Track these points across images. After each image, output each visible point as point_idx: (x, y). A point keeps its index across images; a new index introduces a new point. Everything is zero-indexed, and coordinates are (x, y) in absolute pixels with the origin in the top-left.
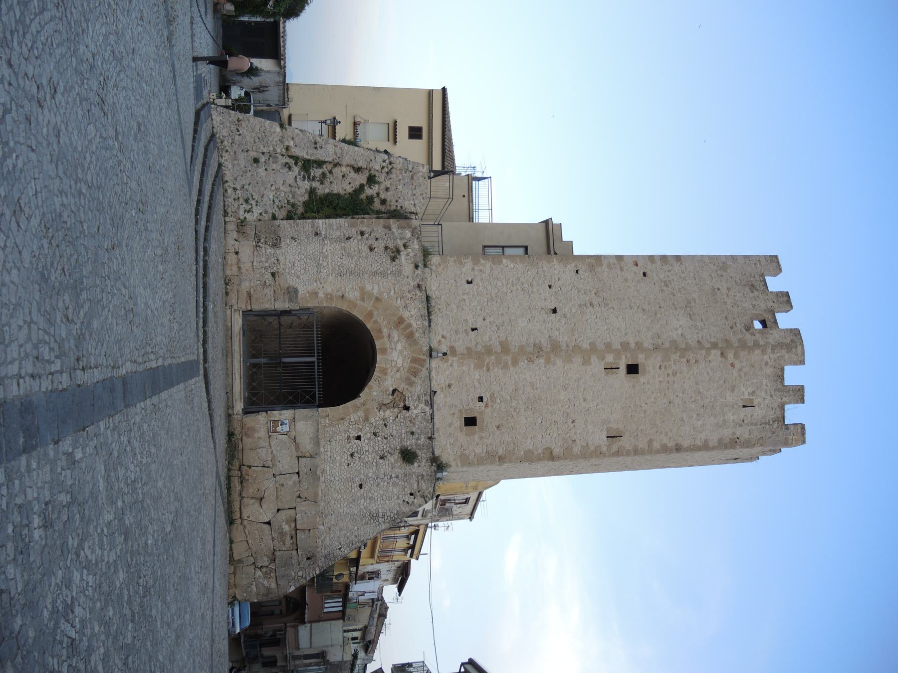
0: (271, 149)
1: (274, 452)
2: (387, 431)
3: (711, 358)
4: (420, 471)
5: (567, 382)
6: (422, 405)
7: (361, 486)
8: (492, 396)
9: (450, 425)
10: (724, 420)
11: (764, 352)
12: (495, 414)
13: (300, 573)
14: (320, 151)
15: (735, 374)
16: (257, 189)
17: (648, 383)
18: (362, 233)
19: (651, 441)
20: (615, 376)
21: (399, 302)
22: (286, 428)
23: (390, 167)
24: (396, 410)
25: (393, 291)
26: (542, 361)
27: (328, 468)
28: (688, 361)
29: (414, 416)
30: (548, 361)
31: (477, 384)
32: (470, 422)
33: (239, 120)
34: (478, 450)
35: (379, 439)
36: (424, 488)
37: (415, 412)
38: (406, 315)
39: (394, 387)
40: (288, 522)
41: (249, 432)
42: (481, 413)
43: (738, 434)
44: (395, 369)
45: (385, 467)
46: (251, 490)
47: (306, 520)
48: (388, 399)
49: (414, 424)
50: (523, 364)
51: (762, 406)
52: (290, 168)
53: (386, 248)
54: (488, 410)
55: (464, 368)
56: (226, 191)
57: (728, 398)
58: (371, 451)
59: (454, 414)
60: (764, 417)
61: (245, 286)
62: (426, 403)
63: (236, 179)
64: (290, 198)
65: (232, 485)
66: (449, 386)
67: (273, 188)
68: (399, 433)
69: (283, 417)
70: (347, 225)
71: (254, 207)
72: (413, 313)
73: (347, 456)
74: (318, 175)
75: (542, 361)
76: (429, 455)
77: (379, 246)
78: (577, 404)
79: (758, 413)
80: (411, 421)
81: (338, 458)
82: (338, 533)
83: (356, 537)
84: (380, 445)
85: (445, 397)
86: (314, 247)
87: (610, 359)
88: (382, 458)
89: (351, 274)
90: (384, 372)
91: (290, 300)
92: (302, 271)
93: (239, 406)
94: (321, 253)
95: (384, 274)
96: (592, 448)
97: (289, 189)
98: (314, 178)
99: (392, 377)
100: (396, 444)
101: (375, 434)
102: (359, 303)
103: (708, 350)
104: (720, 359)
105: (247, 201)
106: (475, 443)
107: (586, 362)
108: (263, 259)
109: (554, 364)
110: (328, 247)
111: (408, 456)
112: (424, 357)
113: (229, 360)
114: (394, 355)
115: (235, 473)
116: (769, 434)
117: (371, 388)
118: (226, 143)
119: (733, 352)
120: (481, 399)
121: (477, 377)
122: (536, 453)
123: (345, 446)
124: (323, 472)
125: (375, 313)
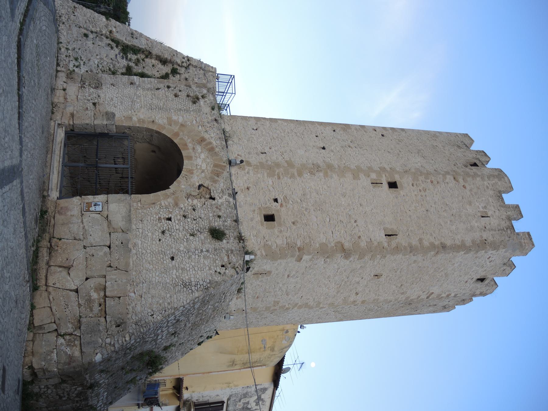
0: (98, 29)
1: (86, 227)
2: (196, 214)
3: (447, 181)
4: (229, 246)
5: (344, 191)
6: (226, 197)
7: (172, 258)
8: (285, 198)
9: (252, 220)
10: (471, 226)
11: (483, 179)
12: (290, 213)
13: (108, 340)
14: (135, 40)
15: (469, 193)
16: (85, 54)
17: (407, 195)
18: (168, 87)
19: (421, 240)
20: (380, 189)
21: (200, 128)
22: (99, 208)
23: (188, 63)
24: (203, 200)
25: (194, 122)
26: (321, 174)
27: (140, 242)
28: (432, 182)
29: (219, 204)
30: (326, 175)
31: (271, 189)
32: (269, 218)
33: (75, 7)
34: (279, 242)
35: (189, 220)
36: (235, 260)
37: (220, 201)
38: (206, 136)
39: (200, 183)
40: (97, 290)
41: (61, 211)
42: (278, 211)
43: (485, 237)
44: (200, 171)
45: (195, 243)
46: (59, 259)
47: (116, 287)
48: (196, 192)
49: (220, 210)
50: (307, 175)
51: (495, 217)
52: (112, 48)
53: (188, 96)
54: (283, 209)
55: (259, 175)
56: (60, 49)
57: (469, 210)
58: (181, 229)
59: (254, 211)
60: (499, 225)
61: (70, 109)
62: (229, 195)
63: (69, 43)
64: (111, 67)
65: (40, 254)
66: (248, 188)
67: (98, 57)
68: (206, 216)
69: (96, 200)
70: (156, 82)
71: (82, 65)
72: (212, 135)
73: (158, 234)
74: (133, 59)
75: (321, 174)
76: (236, 234)
77: (183, 95)
78: (356, 208)
79: (494, 222)
80: (217, 208)
81: (150, 234)
82: (150, 300)
83: (169, 304)
84: (190, 225)
85: (245, 196)
86: (130, 90)
87: (374, 176)
88: (192, 235)
89: (160, 109)
90: (191, 172)
91: (108, 119)
92: (119, 104)
93: (54, 194)
94: (135, 94)
95: (187, 111)
96: (376, 243)
97: (111, 61)
98: (130, 60)
99: (198, 176)
100: (205, 224)
101: (185, 216)
102: (167, 126)
103: (444, 176)
104: (454, 182)
105: (76, 59)
106: (275, 235)
107: (356, 177)
108: (87, 95)
109: (332, 177)
110: (140, 92)
111: (217, 234)
112: (225, 164)
113: (49, 156)
114: (199, 161)
115: (45, 243)
116: (507, 239)
117: (180, 182)
118: (63, 18)
119: (461, 177)
120: (276, 200)
121: (271, 183)
122: (329, 246)
123: (156, 225)
124: (135, 245)
125: (181, 133)
